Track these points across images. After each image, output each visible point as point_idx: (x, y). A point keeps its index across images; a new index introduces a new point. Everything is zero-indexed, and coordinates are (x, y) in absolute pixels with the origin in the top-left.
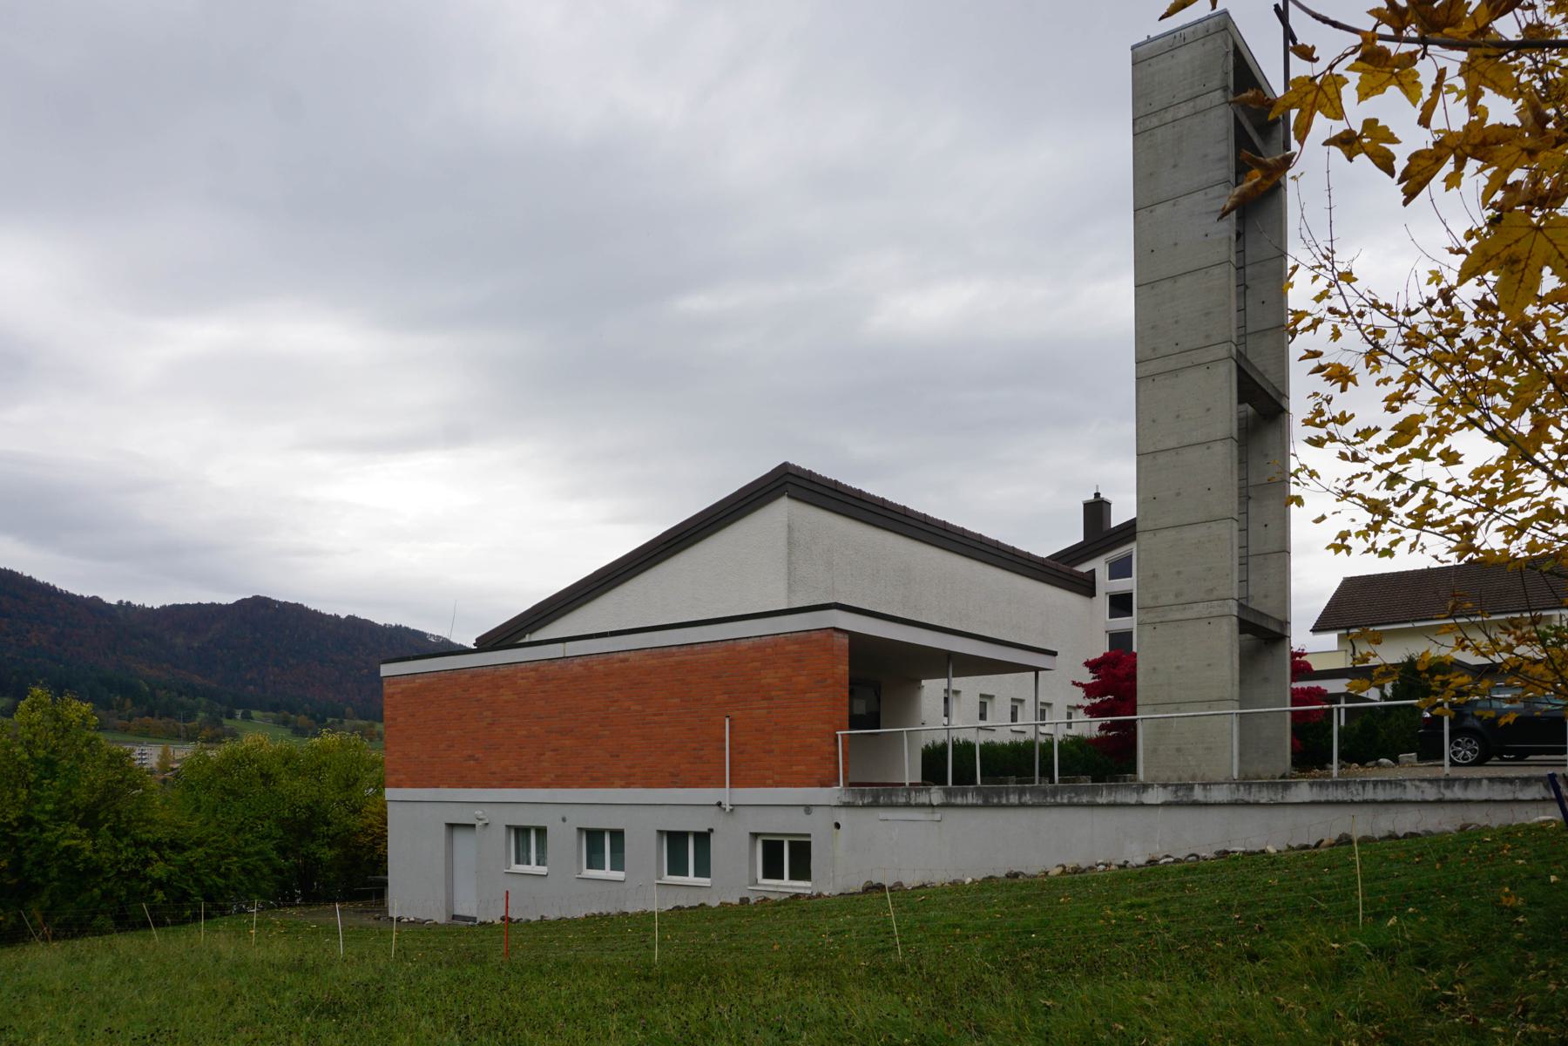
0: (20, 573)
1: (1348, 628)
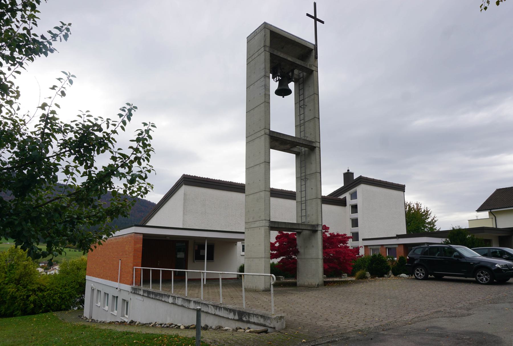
1: (490, 210)
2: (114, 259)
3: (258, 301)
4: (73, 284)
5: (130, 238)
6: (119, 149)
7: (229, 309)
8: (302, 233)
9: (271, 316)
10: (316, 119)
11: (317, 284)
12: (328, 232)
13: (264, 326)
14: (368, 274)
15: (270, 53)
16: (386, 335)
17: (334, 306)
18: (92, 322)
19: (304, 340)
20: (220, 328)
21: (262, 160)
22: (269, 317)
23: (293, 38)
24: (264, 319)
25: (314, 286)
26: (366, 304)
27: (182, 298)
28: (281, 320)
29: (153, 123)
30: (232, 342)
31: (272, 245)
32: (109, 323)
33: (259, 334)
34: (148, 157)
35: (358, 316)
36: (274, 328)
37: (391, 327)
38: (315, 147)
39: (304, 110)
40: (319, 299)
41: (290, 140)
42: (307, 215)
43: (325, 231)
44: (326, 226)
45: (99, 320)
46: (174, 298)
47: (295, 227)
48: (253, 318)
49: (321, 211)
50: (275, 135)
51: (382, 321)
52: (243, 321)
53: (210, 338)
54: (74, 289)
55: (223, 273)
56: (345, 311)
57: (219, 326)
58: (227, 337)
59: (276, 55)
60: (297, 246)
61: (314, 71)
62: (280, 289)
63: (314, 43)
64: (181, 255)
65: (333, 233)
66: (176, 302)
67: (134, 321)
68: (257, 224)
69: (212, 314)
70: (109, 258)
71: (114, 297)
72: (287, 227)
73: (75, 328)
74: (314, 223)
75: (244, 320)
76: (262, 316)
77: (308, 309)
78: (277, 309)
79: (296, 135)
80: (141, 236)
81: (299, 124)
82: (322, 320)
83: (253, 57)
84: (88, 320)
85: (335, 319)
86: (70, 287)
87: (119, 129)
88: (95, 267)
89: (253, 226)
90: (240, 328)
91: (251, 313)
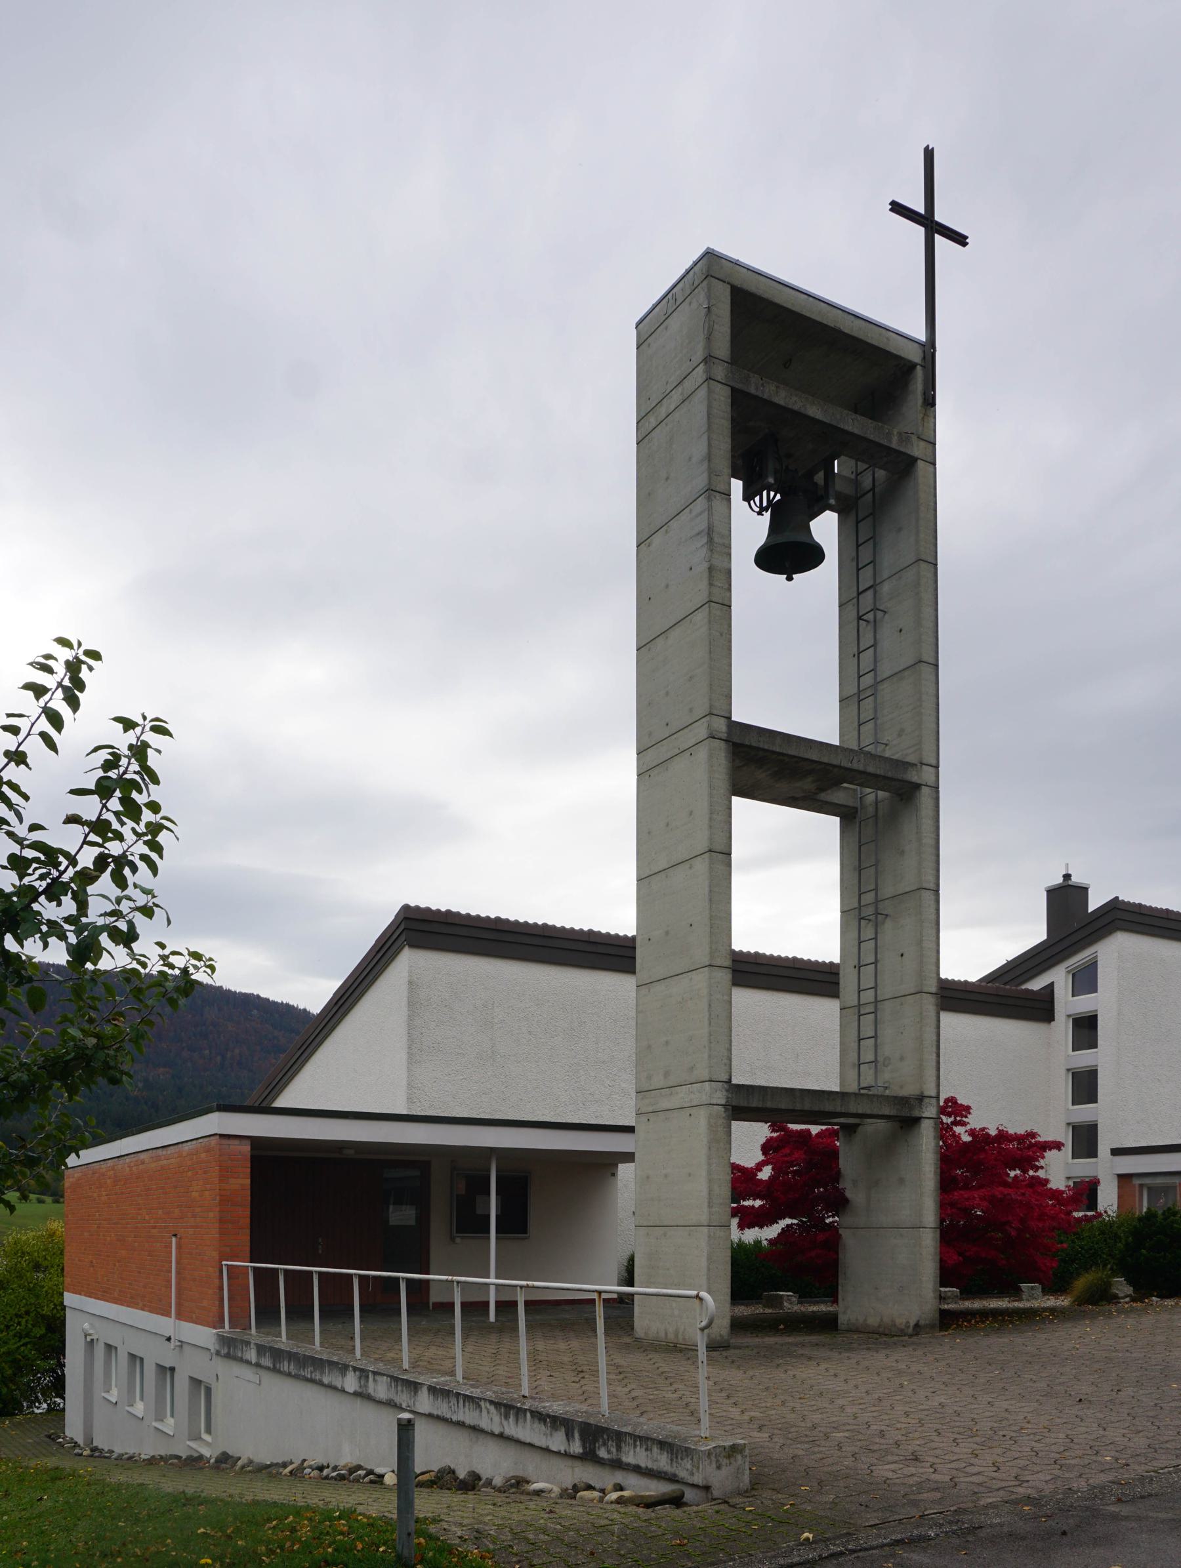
0: (296, 1006)
2: (154, 1231)
3: (675, 1386)
4: (23, 1322)
5: (203, 1155)
6: (34, 827)
7: (548, 1416)
8: (861, 1126)
9: (696, 1443)
10: (926, 670)
11: (912, 1323)
12: (964, 1124)
13: (672, 1479)
14: (1121, 1287)
15: (733, 390)
16: (1126, 1518)
17: (956, 1408)
18: (91, 1456)
19: (806, 1535)
20: (518, 1484)
21: (701, 842)
22: (687, 1449)
23: (830, 319)
24: (672, 1454)
25: (902, 1330)
26: (1080, 1400)
27: (388, 1376)
28: (732, 1460)
29: (157, 719)
30: (541, 1536)
31: (743, 1181)
32: (148, 1460)
33: (651, 1510)
34: (154, 856)
35: (1038, 1446)
36: (707, 1488)
37: (1155, 1488)
38: (917, 786)
39: (875, 632)
40: (910, 1380)
41: (814, 758)
42: (880, 1059)
43: (952, 1119)
44: (959, 1102)
45: (118, 1450)
46: (363, 1374)
47: (828, 1107)
48: (632, 1453)
49: (935, 1043)
50: (753, 741)
51: (1128, 1465)
52: (599, 1462)
53: (465, 1522)
54: (27, 1340)
55: (528, 1286)
56: (996, 1425)
57: (518, 1477)
58: (529, 1519)
59: (755, 397)
60: (841, 1181)
61: (919, 461)
62: (770, 1340)
63: (921, 336)
64: (402, 1216)
65: (983, 1129)
66: (371, 1391)
67: (232, 1457)
68: (682, 1097)
69: (492, 1434)
70: (137, 1227)
71: (161, 1369)
72: (798, 1107)
73: (21, 1481)
74: (909, 1090)
75: (603, 1459)
76: (663, 1445)
77: (856, 1418)
78: (738, 1417)
79: (842, 735)
81: (856, 691)
82: (896, 1458)
83: (663, 411)
84: (80, 1451)
85: (947, 1457)
86: (11, 1333)
87: (34, 747)
88: (92, 1262)
89: (665, 1104)
90: (589, 1487)
91: (626, 1433)
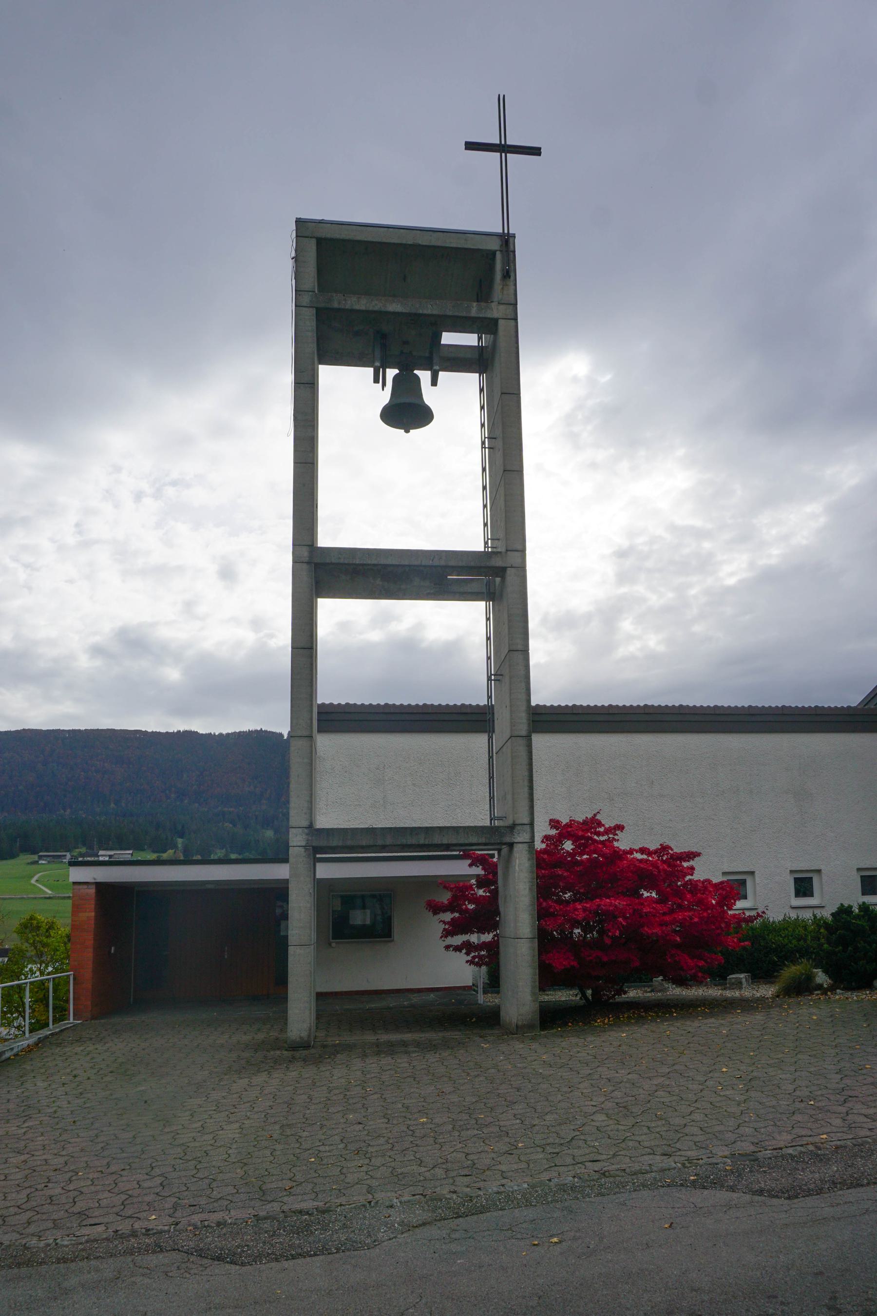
14: (821, 977)
80: (91, 890)
